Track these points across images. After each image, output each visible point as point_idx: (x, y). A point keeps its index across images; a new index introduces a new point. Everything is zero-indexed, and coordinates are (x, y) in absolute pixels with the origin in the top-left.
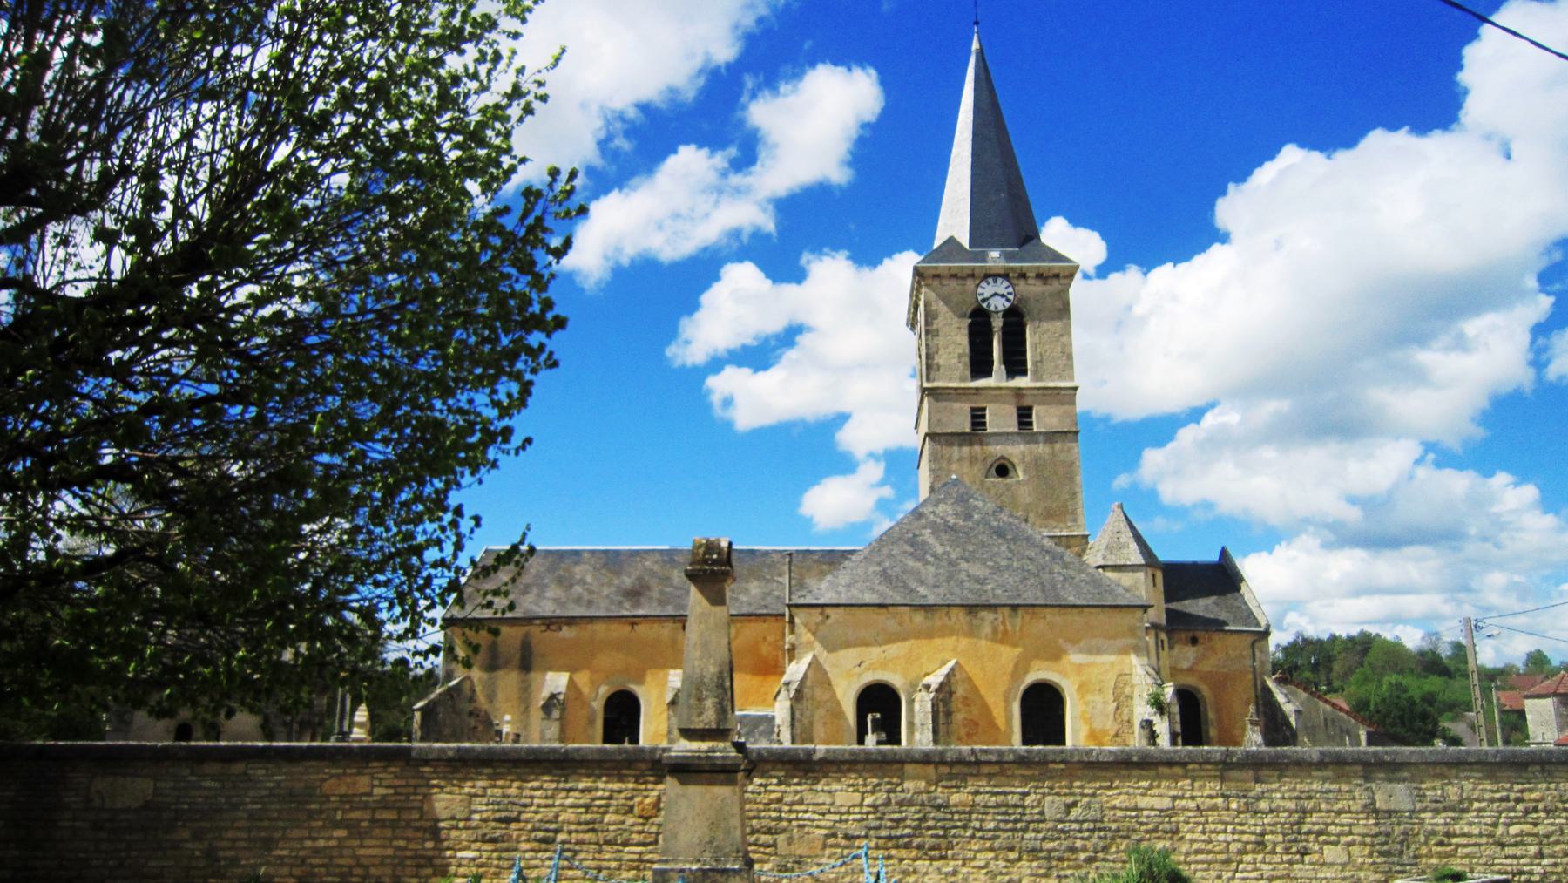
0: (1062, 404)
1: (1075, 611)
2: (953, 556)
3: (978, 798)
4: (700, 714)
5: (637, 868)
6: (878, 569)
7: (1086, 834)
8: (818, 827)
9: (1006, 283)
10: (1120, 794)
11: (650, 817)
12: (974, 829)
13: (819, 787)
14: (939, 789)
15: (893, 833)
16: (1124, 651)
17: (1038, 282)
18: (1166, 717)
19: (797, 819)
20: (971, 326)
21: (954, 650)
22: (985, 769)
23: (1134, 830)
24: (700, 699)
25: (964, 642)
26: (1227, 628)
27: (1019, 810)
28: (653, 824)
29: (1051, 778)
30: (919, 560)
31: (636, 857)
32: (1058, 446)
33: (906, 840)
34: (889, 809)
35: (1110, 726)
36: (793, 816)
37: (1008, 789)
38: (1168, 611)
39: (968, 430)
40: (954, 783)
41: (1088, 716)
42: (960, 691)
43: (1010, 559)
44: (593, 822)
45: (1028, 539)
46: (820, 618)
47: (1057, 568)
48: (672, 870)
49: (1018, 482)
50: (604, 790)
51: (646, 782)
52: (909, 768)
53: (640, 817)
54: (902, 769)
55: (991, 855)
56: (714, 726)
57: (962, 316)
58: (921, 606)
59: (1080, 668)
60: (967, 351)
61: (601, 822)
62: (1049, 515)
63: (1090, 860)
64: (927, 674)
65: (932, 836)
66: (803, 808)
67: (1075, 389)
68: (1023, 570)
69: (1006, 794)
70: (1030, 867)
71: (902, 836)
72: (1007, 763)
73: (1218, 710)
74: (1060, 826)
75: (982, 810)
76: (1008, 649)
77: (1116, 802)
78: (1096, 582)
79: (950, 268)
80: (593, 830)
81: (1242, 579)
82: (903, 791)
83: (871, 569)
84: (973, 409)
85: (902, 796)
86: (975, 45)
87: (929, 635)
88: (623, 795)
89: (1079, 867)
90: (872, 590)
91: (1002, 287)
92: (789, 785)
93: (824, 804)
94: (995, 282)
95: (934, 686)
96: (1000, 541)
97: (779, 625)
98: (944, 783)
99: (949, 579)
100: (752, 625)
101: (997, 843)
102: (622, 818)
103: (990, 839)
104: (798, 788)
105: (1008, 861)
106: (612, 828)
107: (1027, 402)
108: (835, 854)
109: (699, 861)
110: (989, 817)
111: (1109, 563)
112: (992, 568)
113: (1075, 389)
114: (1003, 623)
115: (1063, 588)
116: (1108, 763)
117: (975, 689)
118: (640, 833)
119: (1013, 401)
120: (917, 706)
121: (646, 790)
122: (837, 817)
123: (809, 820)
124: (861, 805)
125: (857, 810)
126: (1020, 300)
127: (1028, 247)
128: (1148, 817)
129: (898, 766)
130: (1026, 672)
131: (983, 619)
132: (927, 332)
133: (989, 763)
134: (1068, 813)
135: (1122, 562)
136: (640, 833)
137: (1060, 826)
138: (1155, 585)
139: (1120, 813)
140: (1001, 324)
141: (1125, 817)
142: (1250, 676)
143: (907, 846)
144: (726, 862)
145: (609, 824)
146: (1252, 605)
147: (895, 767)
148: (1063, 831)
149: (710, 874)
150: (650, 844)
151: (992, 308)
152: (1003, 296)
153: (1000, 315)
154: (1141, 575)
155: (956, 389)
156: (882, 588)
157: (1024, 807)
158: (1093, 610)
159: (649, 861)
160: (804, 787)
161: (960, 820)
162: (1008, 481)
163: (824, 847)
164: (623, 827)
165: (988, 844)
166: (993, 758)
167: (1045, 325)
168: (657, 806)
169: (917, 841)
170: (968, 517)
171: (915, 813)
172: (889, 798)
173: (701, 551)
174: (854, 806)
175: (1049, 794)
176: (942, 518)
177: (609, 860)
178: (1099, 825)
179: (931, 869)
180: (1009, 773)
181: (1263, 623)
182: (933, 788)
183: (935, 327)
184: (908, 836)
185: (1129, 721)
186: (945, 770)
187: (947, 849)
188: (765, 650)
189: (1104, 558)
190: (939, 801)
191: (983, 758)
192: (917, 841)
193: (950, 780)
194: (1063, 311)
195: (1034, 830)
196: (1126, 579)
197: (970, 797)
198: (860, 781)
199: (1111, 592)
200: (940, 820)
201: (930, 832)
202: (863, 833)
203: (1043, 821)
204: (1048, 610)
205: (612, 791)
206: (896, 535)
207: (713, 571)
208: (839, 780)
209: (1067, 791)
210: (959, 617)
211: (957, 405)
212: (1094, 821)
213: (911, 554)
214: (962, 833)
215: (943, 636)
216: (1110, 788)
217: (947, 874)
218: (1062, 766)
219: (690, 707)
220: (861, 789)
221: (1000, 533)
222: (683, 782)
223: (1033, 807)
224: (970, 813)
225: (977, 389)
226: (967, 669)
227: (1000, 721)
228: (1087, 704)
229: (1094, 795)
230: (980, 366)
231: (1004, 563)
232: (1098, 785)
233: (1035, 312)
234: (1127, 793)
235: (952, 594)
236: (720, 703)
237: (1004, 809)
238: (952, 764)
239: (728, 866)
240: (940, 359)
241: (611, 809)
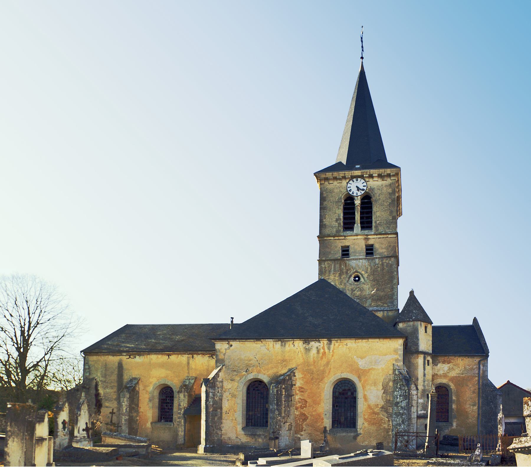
9: (363, 181)
17: (380, 180)
46: (228, 346)
73: (458, 396)
126: (370, 189)
138: (426, 332)
142: (477, 378)
151: (355, 195)
153: (359, 197)
230: (348, 225)
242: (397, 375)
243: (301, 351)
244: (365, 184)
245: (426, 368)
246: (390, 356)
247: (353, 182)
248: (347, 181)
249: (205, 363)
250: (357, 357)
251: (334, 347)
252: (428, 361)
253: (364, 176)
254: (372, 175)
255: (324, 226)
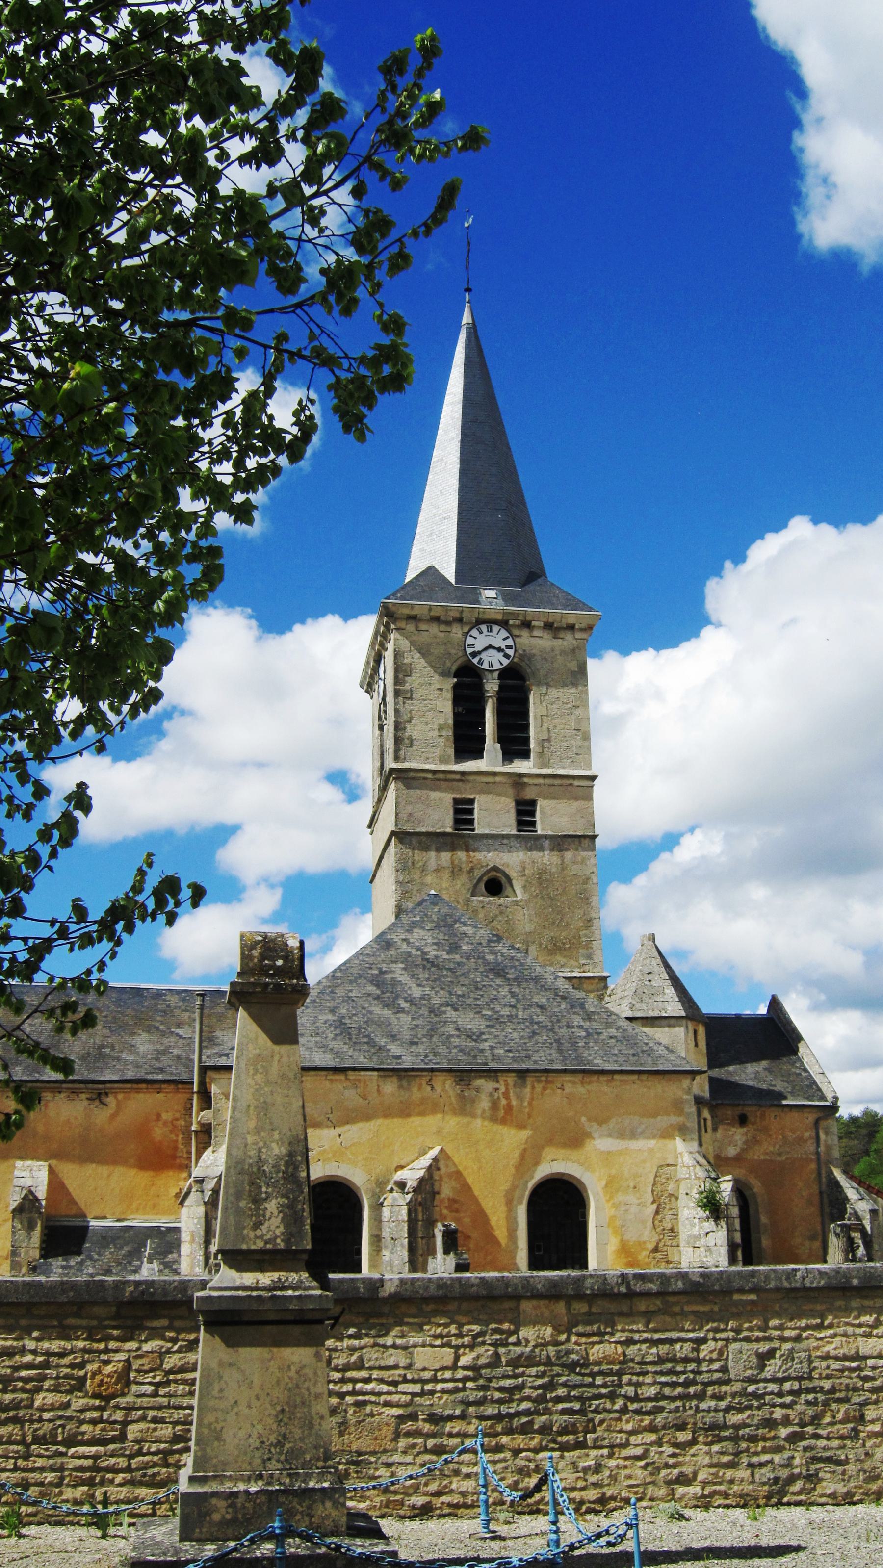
0: (576, 799)
1: (603, 1078)
2: (436, 1001)
3: (632, 1350)
4: (257, 1225)
5: (90, 1483)
6: (330, 1017)
7: (788, 1399)
8: (387, 1404)
10: (835, 1335)
11: (114, 1396)
12: (625, 1397)
13: (389, 1341)
14: (574, 1339)
15: (504, 1409)
16: (666, 1134)
17: (546, 635)
18: (723, 1223)
19: (353, 1393)
20: (456, 687)
21: (439, 1132)
22: (642, 1306)
23: (855, 1389)
24: (257, 1201)
25: (452, 1122)
26: (785, 1102)
27: (692, 1366)
28: (117, 1407)
29: (736, 1316)
30: (387, 1006)
31: (88, 1463)
32: (568, 855)
33: (524, 1420)
34: (499, 1371)
35: (649, 1237)
36: (348, 1387)
37: (674, 1335)
38: (712, 1080)
39: (449, 830)
40: (595, 1327)
41: (618, 1223)
42: (446, 1191)
43: (514, 1007)
44: (16, 1405)
45: (536, 980)
47: (577, 1020)
48: (214, 1494)
49: (516, 903)
50: (34, 1352)
51: (107, 1339)
52: (526, 1306)
53: (95, 1396)
54: (518, 1306)
55: (652, 1437)
56: (282, 1246)
57: (444, 674)
58: (393, 1070)
59: (608, 1157)
60: (451, 722)
61: (31, 1406)
62: (556, 948)
63: (794, 1438)
64: (402, 1167)
65: (564, 1412)
66: (364, 1374)
67: (593, 778)
68: (532, 1022)
69: (671, 1342)
70: (708, 1453)
71: (518, 1414)
72: (674, 1293)
74: (751, 1389)
75: (638, 1368)
76: (513, 1131)
77: (830, 1348)
78: (628, 1040)
79: (430, 608)
80: (15, 1420)
81: (799, 1038)
82: (518, 1343)
83: (322, 1018)
84: (456, 801)
85: (518, 1350)
86: (466, 318)
87: (405, 1111)
88: (66, 1361)
89: (779, 1450)
90: (324, 1047)
91: (499, 637)
92: (340, 1339)
93: (396, 1367)
94: (490, 630)
95: (411, 1184)
96: (499, 981)
97: (182, 1097)
98: (580, 1329)
99: (432, 1032)
100: (141, 1096)
101: (660, 1419)
102: (65, 1398)
103: (648, 1413)
104: (356, 1343)
105: (676, 1445)
106: (47, 1416)
107: (529, 794)
108: (414, 1446)
109: (260, 1477)
110: (648, 1379)
111: (639, 1014)
112: (489, 1018)
113: (593, 778)
114: (506, 1095)
115: (586, 1046)
116: (817, 1289)
117: (466, 1188)
118: (94, 1422)
119: (511, 791)
120: (386, 1212)
121: (106, 1351)
122: (417, 1388)
123: (373, 1393)
124: (454, 1367)
125: (448, 1375)
126: (522, 657)
127: (531, 587)
128: (874, 1368)
129: (511, 1304)
130: (537, 1163)
131: (478, 1090)
132: (397, 693)
133: (647, 1294)
134: (762, 1367)
135: (655, 1014)
136: (94, 1422)
137: (751, 1389)
138: (696, 1045)
139: (836, 1365)
140: (496, 688)
141: (842, 1371)
142: (813, 1166)
143: (525, 1430)
144: (308, 1477)
145: (42, 1409)
146: (813, 1071)
147: (507, 1305)
148: (755, 1395)
149: (282, 1499)
150: (113, 1440)
151: (485, 666)
152: (499, 650)
153: (496, 674)
154: (679, 1032)
155: (434, 772)
156: (338, 1045)
157: (699, 1361)
158: (625, 1077)
159: (108, 1470)
160: (365, 1341)
161: (605, 1386)
162: (502, 901)
163: (397, 1436)
164: (68, 1413)
165: (647, 1420)
166: (653, 1287)
167: (554, 693)
168: (124, 1378)
169: (540, 1421)
170: (454, 948)
171: (537, 1376)
172: (497, 1355)
173: (256, 953)
174: (443, 1369)
175: (735, 1340)
176: (418, 949)
177: (42, 1470)
178: (806, 1384)
179: (562, 1464)
180: (677, 1309)
181: (829, 1096)
182: (563, 1337)
183: (407, 687)
184: (527, 1413)
185: (672, 1230)
186: (581, 1307)
187: (586, 1432)
188: (158, 1132)
189: (632, 1007)
190: (574, 1357)
191: (638, 1287)
192: (540, 1421)
193: (590, 1323)
194: (579, 676)
195: (714, 1397)
196: (661, 1034)
197: (620, 1349)
198: (453, 1329)
199: (650, 1052)
200: (575, 1387)
201: (560, 1406)
202: (458, 1412)
203: (727, 1382)
204: (567, 1077)
205: (48, 1354)
206: (355, 971)
207: (278, 986)
208: (419, 1328)
209: (761, 1334)
210: (446, 1086)
211: (435, 795)
212: (799, 1379)
213: (378, 998)
214: (608, 1405)
215: (422, 1114)
216: (820, 1327)
217: (586, 1470)
218: (753, 1297)
219: (239, 1212)
220: (454, 1341)
221: (499, 971)
222: (231, 1342)
223: (712, 1361)
224: (620, 1374)
225: (463, 773)
226: (456, 1160)
227: (501, 1234)
228: (616, 1206)
229: (798, 1339)
231: (506, 1012)
232: (803, 1323)
233: (542, 672)
234: (845, 1335)
235: (436, 1054)
236: (291, 1206)
237: (669, 1366)
238: (592, 1298)
239: (311, 1484)
240: (414, 731)
241: (47, 1384)
242: (688, 1167)
243: (451, 1104)
244: (510, 642)
245: (703, 1139)
246: (665, 1118)
247: (481, 633)
248: (466, 629)
249: (76, 1118)
250: (589, 1120)
251: (532, 1093)
252: (705, 1120)
253: (511, 622)
254: (530, 622)
255: (407, 741)
